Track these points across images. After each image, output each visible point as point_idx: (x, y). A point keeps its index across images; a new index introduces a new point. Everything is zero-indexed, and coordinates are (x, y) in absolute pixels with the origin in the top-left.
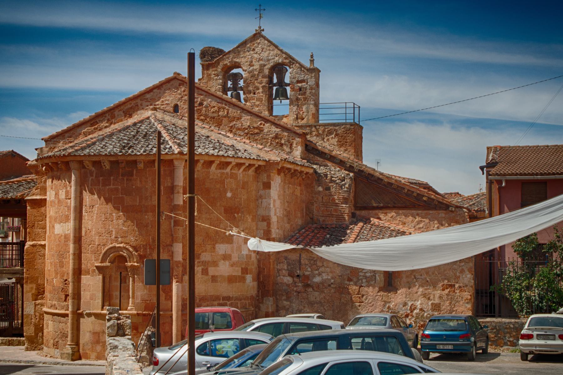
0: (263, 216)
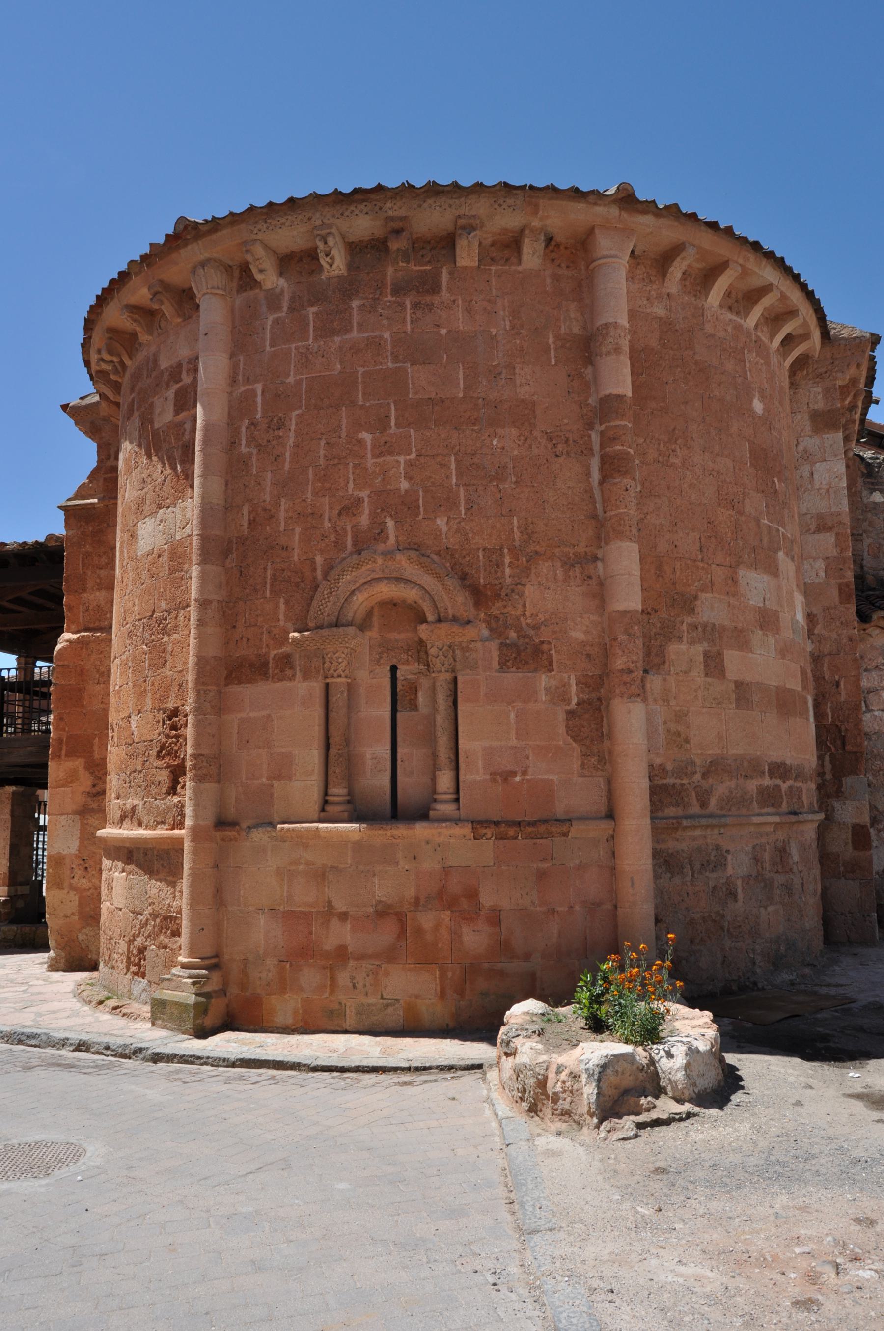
0: (820, 516)
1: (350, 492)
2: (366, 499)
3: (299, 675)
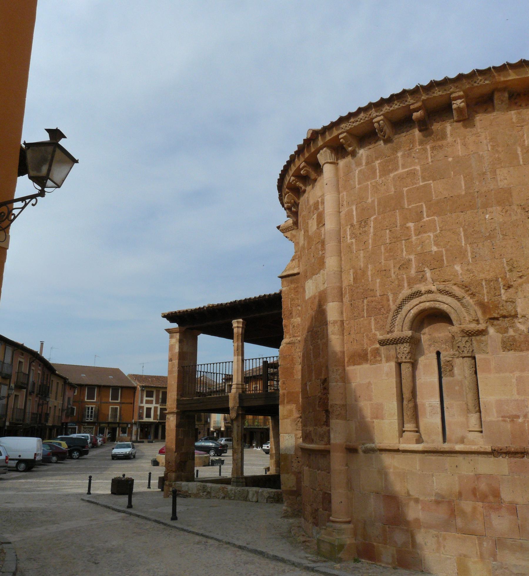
2: (413, 260)
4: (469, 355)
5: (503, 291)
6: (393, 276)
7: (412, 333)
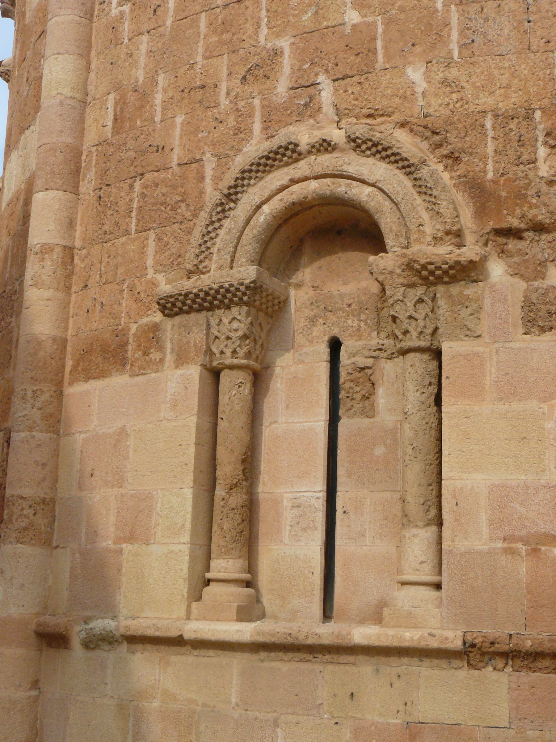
1: (262, 39)
2: (287, 52)
3: (169, 358)
4: (423, 343)
5: (542, 152)
6: (224, 102)
7: (259, 274)
